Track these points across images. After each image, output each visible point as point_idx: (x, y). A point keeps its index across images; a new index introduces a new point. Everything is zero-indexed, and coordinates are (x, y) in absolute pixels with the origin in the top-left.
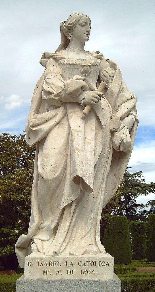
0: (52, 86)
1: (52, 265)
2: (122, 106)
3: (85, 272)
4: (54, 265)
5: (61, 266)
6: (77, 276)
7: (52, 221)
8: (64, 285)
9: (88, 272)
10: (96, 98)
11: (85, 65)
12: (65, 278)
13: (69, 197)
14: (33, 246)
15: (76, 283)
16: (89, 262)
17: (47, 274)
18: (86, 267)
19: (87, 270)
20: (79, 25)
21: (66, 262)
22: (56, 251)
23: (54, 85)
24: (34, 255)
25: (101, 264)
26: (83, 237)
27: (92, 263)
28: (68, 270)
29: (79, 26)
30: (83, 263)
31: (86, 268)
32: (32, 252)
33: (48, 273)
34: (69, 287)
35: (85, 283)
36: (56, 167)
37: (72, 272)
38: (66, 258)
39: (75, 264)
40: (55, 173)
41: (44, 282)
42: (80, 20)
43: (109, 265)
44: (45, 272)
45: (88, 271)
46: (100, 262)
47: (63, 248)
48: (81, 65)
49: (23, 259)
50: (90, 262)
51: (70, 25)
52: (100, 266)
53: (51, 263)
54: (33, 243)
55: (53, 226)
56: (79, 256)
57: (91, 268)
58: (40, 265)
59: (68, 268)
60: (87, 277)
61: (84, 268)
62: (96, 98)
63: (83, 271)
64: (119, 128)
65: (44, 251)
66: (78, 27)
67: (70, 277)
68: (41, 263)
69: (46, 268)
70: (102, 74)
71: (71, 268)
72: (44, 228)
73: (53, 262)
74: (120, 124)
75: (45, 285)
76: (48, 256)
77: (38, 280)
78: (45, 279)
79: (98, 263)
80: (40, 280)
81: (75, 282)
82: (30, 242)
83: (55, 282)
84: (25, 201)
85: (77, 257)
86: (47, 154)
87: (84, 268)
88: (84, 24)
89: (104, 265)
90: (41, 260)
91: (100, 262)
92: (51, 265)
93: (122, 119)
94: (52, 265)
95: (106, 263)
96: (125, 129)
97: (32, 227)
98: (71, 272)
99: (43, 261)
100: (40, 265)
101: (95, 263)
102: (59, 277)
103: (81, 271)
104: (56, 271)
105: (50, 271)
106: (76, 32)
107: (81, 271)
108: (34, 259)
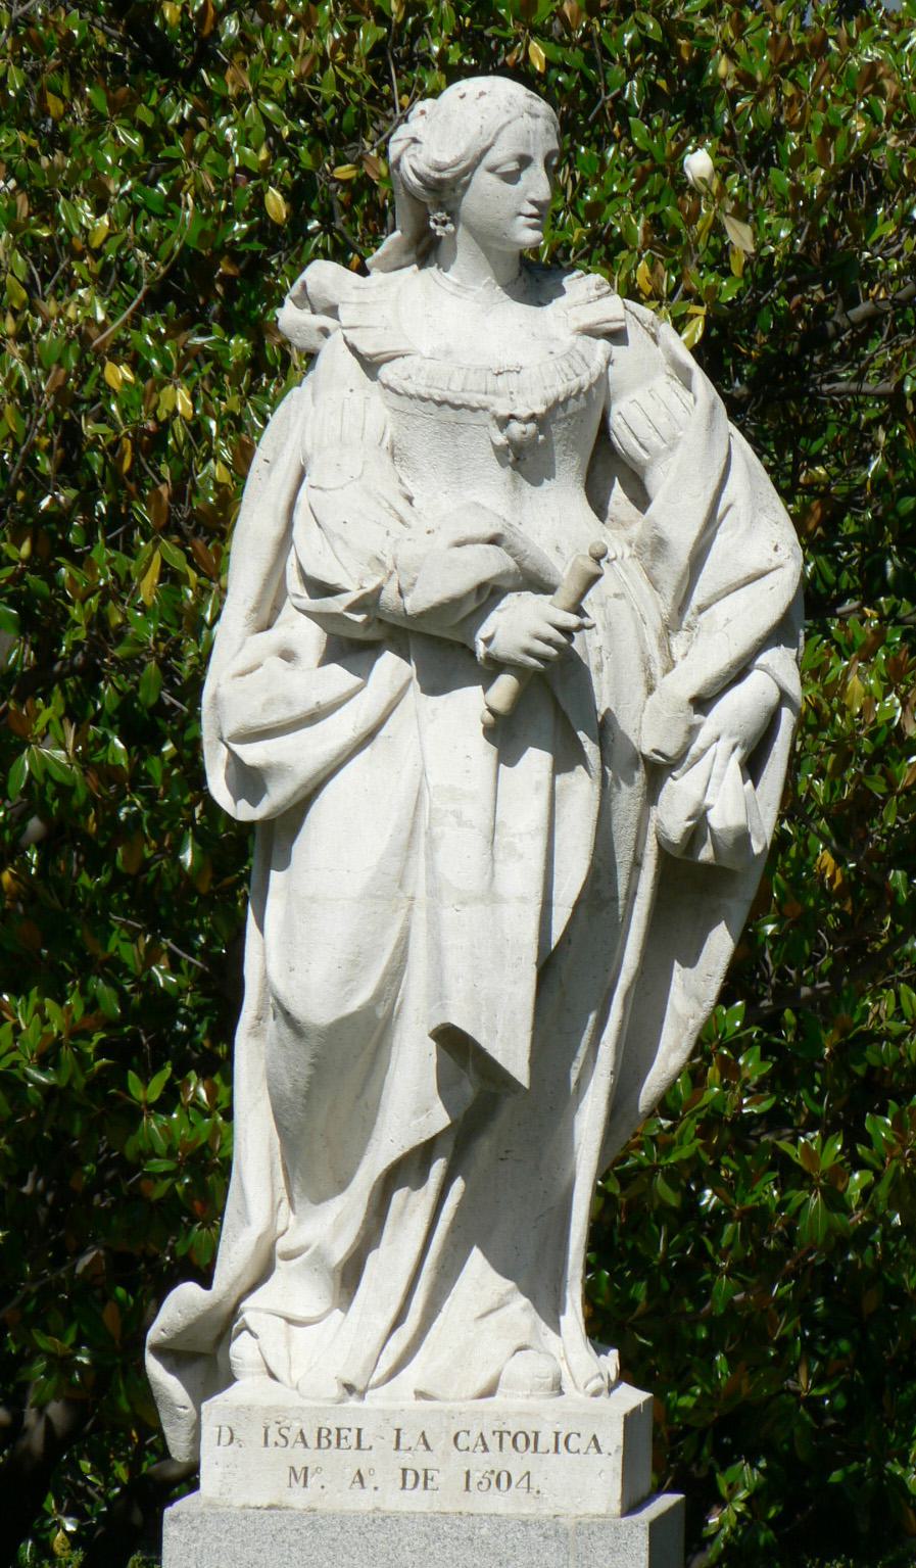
0: (338, 545)
1: (329, 1442)
2: (720, 609)
3: (485, 1482)
4: (339, 1444)
5: (371, 1448)
6: (445, 1497)
7: (338, 1227)
8: (382, 1536)
9: (500, 1480)
10: (548, 641)
11: (512, 417)
12: (393, 1508)
13: (416, 1114)
14: (241, 1350)
15: (441, 1531)
16: (505, 1435)
17: (305, 1485)
18: (495, 1460)
19: (493, 1472)
20: (492, 170)
21: (398, 1430)
22: (349, 1378)
23: (346, 543)
24: (247, 1390)
25: (561, 1442)
26: (491, 1311)
27: (521, 1440)
28: (404, 1471)
29: (491, 178)
30: (475, 1435)
31: (488, 1462)
32: (235, 1380)
33: (310, 1481)
34: (407, 1548)
35: (484, 1531)
36: (354, 964)
37: (424, 1479)
38: (394, 1412)
39: (441, 1443)
40: (352, 993)
41: (292, 1522)
42: (492, 144)
43: (599, 1451)
44: (300, 1476)
45: (499, 1475)
46: (557, 1434)
47: (386, 1363)
48: (492, 409)
49: (187, 1411)
50: (509, 1433)
51: (439, 170)
52: (556, 1450)
53: (324, 1433)
54: (240, 1331)
55: (339, 1251)
56: (458, 1406)
57: (516, 1463)
58: (276, 1444)
59: (406, 1459)
60: (498, 1503)
61: (480, 1464)
62: (548, 641)
63: (476, 1477)
64: (684, 752)
65: (297, 1375)
66: (483, 180)
67: (416, 1501)
68: (276, 1432)
69: (300, 1457)
70: (619, 419)
71: (419, 1460)
72: (299, 1255)
73: (334, 1432)
74: (693, 731)
75: (293, 1537)
76: (314, 1399)
77: (262, 1512)
78: (295, 1506)
79: (547, 1441)
80: (273, 1512)
81: (434, 1526)
82: (224, 1325)
83: (342, 1520)
84: (40, 423)
85: (449, 1406)
86: (313, 899)
87: (480, 1464)
88: (513, 166)
89: (578, 1451)
90: (280, 1419)
91: (557, 1434)
92: (324, 1442)
93: (702, 703)
94: (329, 1442)
95: (586, 1439)
96: (718, 757)
97: (234, 1255)
98: (422, 1479)
99: (287, 1423)
100: (276, 1444)
101: (533, 1441)
102: (362, 1501)
103: (468, 1473)
104: (350, 1473)
105: (318, 1470)
106: (471, 203)
107: (468, 1473)
108: (244, 1411)
